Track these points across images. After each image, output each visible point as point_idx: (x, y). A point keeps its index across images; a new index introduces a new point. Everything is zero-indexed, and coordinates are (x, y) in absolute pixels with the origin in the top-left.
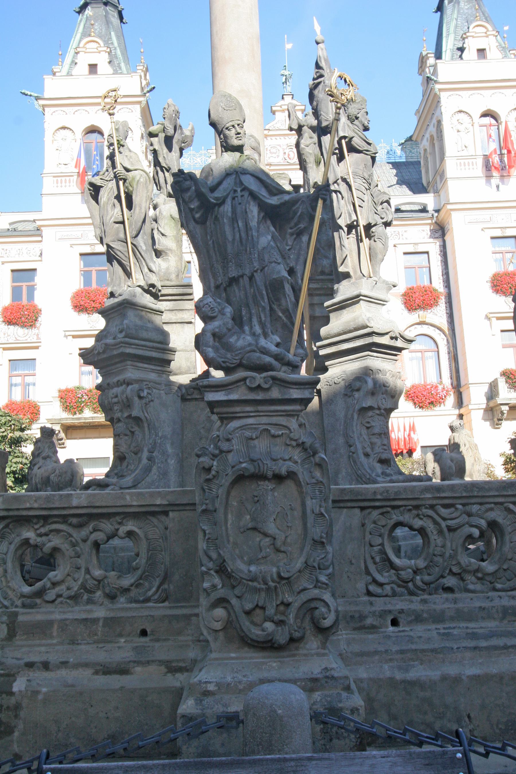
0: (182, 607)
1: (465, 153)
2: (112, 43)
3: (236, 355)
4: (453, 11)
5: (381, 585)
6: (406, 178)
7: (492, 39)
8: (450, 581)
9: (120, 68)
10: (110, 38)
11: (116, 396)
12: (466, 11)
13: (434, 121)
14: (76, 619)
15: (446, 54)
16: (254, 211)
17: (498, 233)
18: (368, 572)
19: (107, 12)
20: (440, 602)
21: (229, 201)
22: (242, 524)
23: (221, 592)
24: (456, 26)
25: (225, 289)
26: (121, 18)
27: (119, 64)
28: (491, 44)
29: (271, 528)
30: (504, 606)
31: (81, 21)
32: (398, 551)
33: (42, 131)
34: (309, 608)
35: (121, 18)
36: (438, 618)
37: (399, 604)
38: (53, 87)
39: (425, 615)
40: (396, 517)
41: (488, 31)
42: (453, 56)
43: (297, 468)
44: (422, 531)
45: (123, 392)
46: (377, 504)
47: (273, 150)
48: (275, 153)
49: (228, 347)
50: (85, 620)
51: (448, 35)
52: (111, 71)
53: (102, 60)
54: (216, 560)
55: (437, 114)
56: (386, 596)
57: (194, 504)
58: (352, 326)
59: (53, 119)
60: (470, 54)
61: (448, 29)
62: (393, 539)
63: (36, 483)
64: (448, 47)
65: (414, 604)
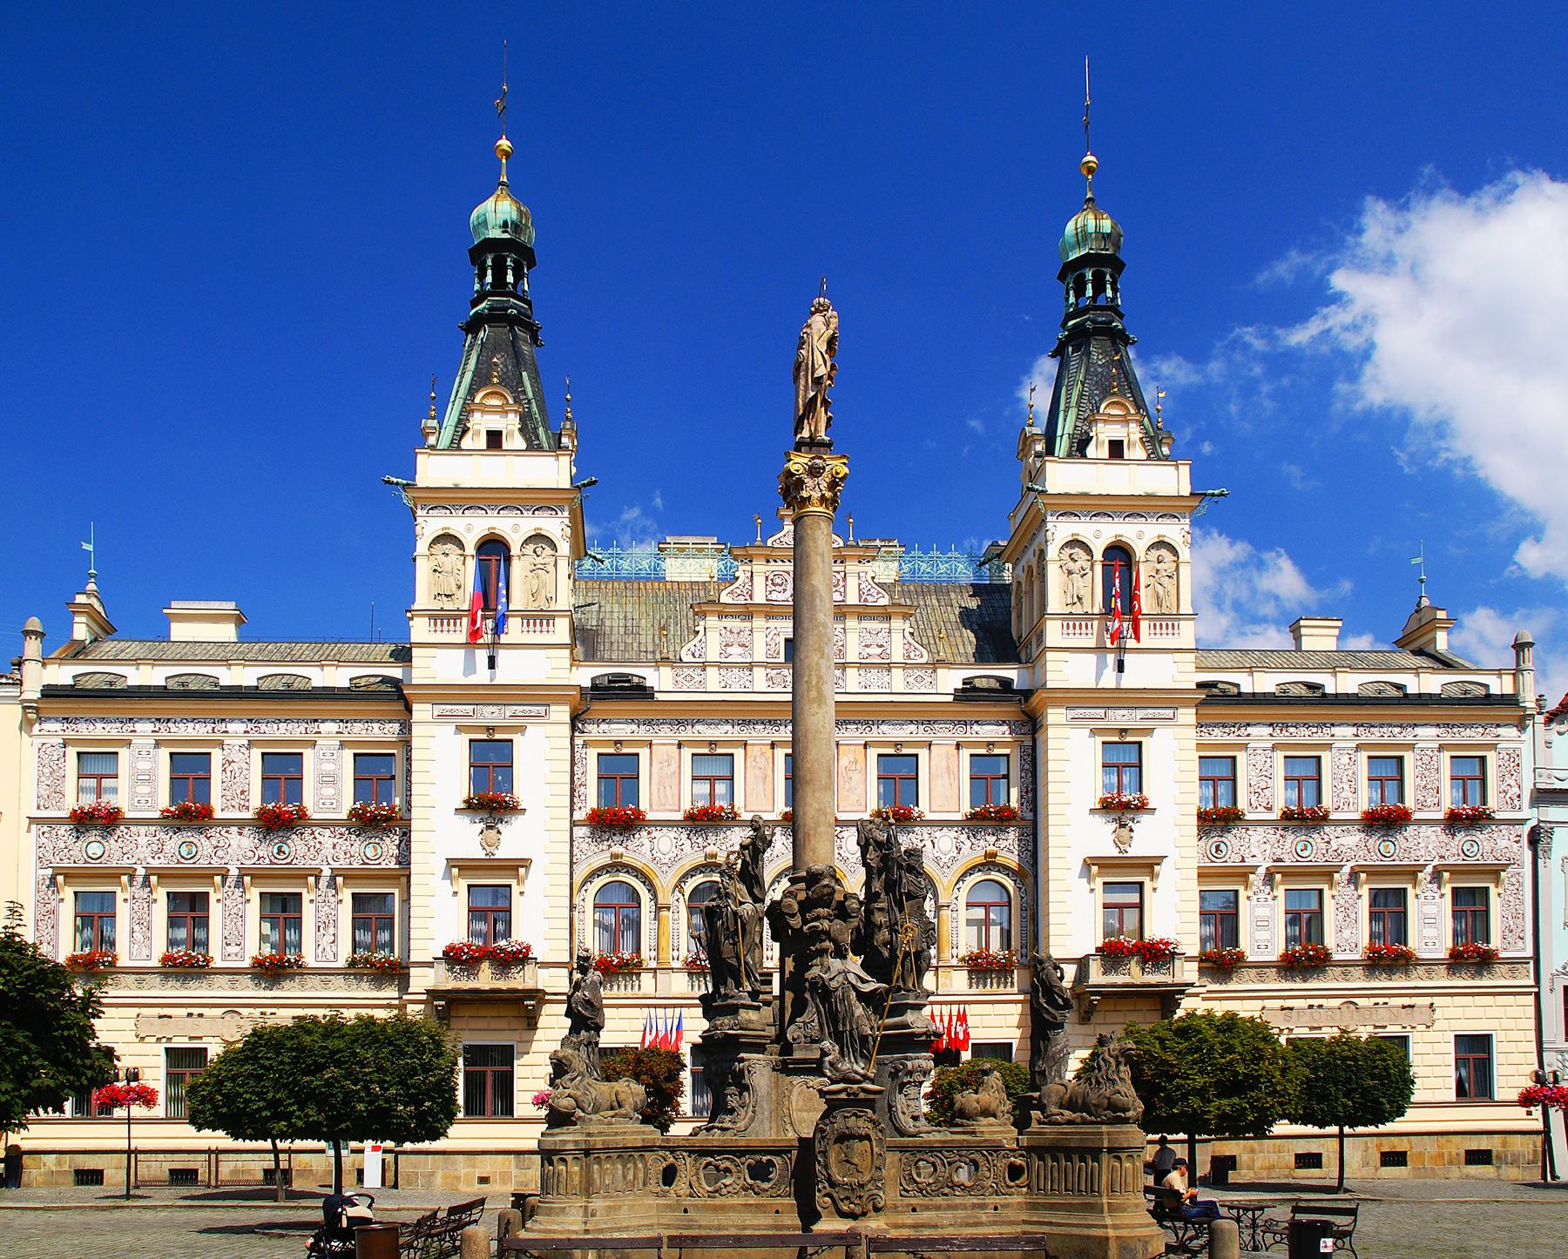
1: (1077, 609)
2: (524, 392)
4: (1079, 368)
7: (1134, 427)
8: (946, 1190)
9: (537, 437)
13: (1034, 546)
15: (1062, 446)
16: (853, 995)
19: (515, 335)
20: (940, 1200)
23: (829, 1190)
24: (1081, 396)
26: (535, 340)
27: (536, 428)
29: (856, 1160)
31: (471, 346)
32: (919, 1175)
33: (413, 539)
34: (872, 1197)
35: (535, 340)
36: (938, 1208)
37: (914, 1201)
38: (433, 470)
40: (919, 1156)
41: (1129, 413)
43: (870, 1133)
44: (934, 1164)
47: (779, 581)
49: (837, 1070)
51: (1066, 411)
52: (524, 446)
53: (509, 424)
55: (1040, 538)
59: (430, 525)
61: (1068, 398)
62: (918, 1168)
65: (926, 1201)
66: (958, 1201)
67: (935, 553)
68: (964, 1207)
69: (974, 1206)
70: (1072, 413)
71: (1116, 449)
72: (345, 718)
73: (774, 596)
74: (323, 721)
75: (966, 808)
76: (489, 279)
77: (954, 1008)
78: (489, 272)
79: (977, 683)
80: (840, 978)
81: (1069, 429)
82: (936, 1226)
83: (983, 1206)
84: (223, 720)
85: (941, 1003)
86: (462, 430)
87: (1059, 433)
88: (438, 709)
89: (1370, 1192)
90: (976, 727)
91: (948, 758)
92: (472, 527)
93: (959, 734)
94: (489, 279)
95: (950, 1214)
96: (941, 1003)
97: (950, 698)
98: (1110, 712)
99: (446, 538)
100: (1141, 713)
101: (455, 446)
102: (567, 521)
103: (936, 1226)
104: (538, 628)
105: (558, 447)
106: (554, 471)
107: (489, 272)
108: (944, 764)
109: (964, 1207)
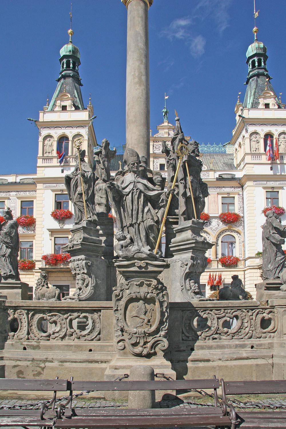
0: (106, 342)
3: (131, 254)
5: (188, 337)
6: (226, 161)
10: (74, 93)
11: (78, 265)
12: (261, 85)
14: (64, 345)
17: (132, 317)
18: (183, 333)
21: (130, 195)
22: (131, 315)
24: (255, 92)
25: (128, 228)
28: (271, 101)
30: (236, 344)
36: (210, 348)
39: (205, 347)
42: (252, 106)
45: (81, 263)
46: (189, 309)
47: (158, 147)
48: (158, 148)
50: (67, 345)
51: (250, 97)
54: (281, 226)
56: (190, 341)
57: (112, 307)
58: (186, 239)
60: (261, 106)
63: (39, 296)
64: (251, 102)
66: (226, 343)
67: (209, 145)
68: (230, 347)
69: (237, 346)
70: (252, 98)
71: (267, 106)
72: (18, 191)
73: (156, 152)
74: (11, 192)
75: (220, 212)
76: (65, 66)
77: (218, 273)
78: (65, 65)
79: (224, 176)
80: (131, 186)
81: (251, 101)
82: (208, 361)
83: (243, 346)
84: (9, 192)
85: (213, 272)
86: (54, 105)
87: (248, 102)
88: (45, 185)
89: (239, 341)
90: (223, 189)
91: (214, 198)
92: (56, 133)
93: (218, 190)
94: (65, 66)
95: (218, 351)
96: (213, 272)
97: (215, 180)
98: (268, 182)
99: (49, 136)
100: (278, 183)
101: (52, 111)
102: (87, 130)
103: (208, 361)
104: (256, 158)
105: (84, 109)
106: (83, 116)
107: (65, 65)
108: (213, 199)
109: (230, 347)
